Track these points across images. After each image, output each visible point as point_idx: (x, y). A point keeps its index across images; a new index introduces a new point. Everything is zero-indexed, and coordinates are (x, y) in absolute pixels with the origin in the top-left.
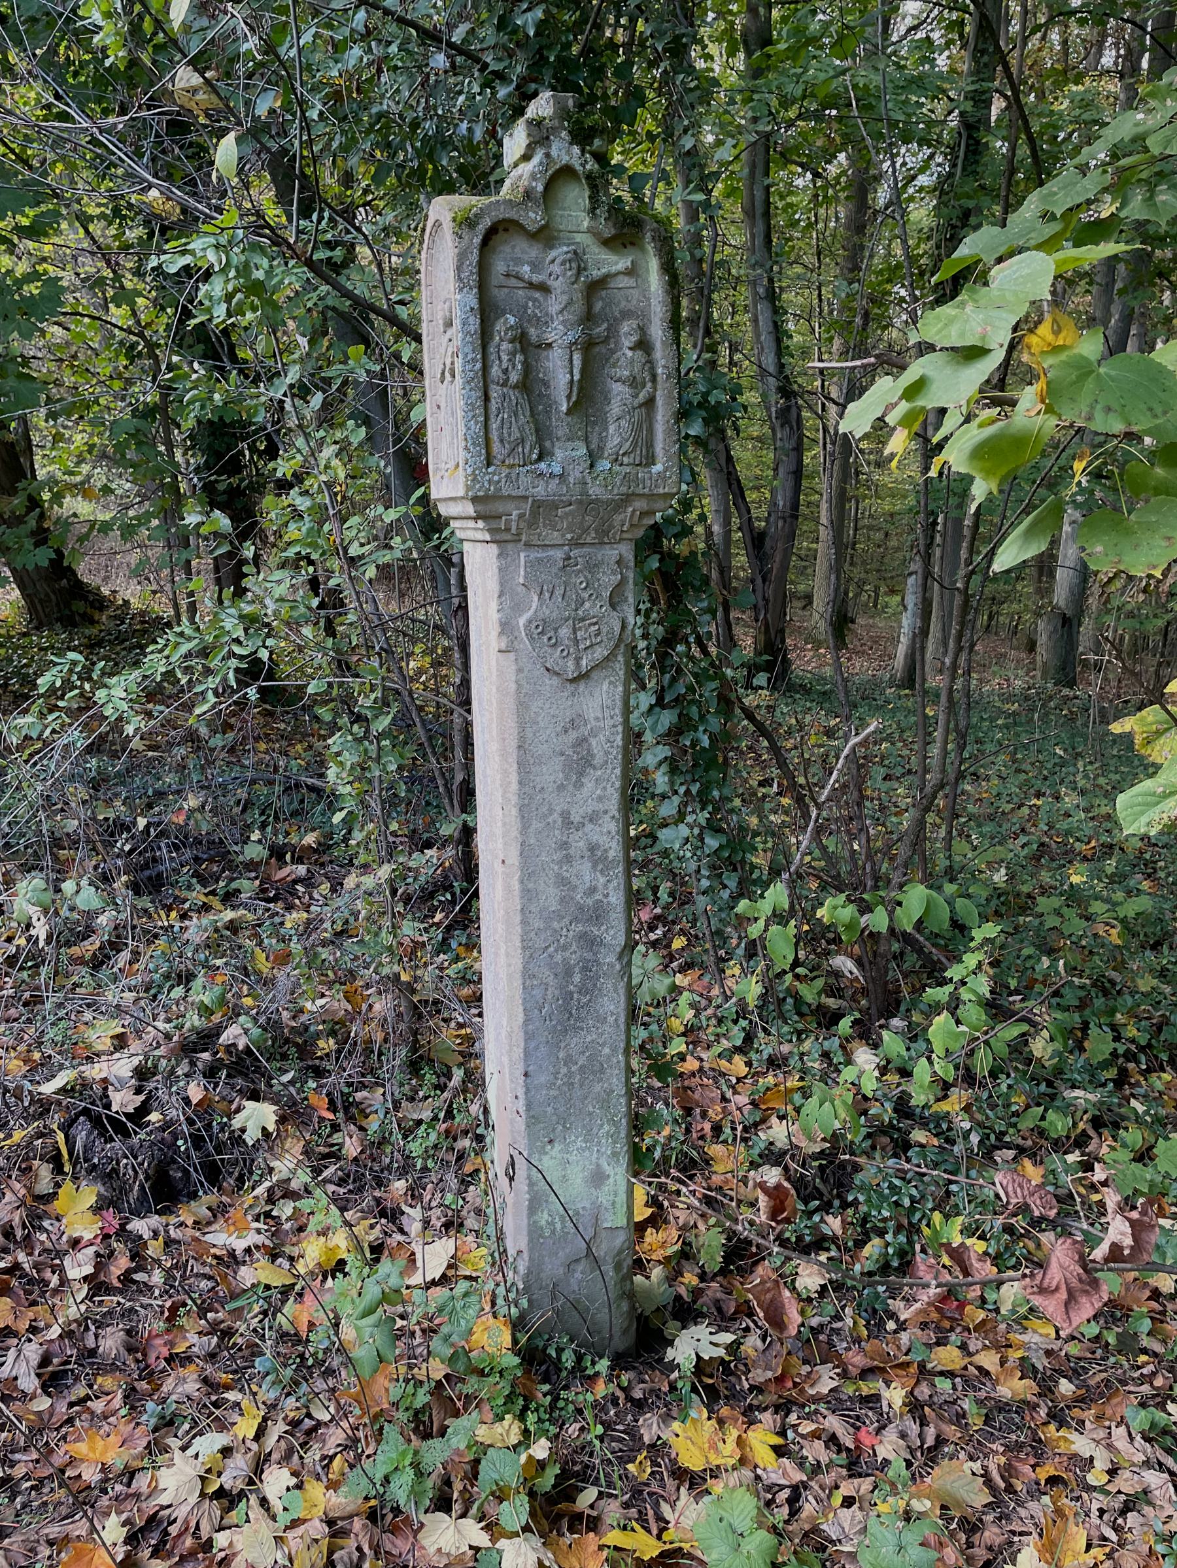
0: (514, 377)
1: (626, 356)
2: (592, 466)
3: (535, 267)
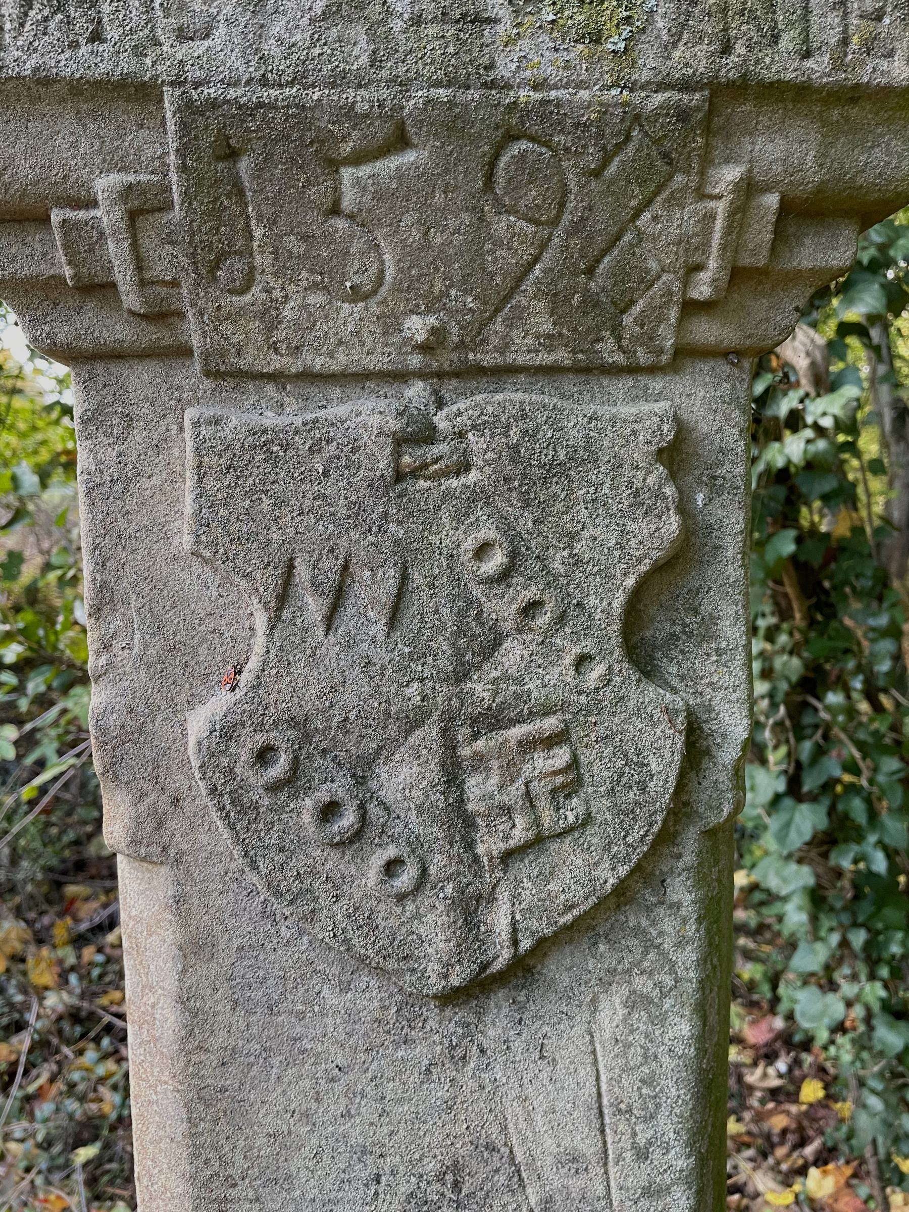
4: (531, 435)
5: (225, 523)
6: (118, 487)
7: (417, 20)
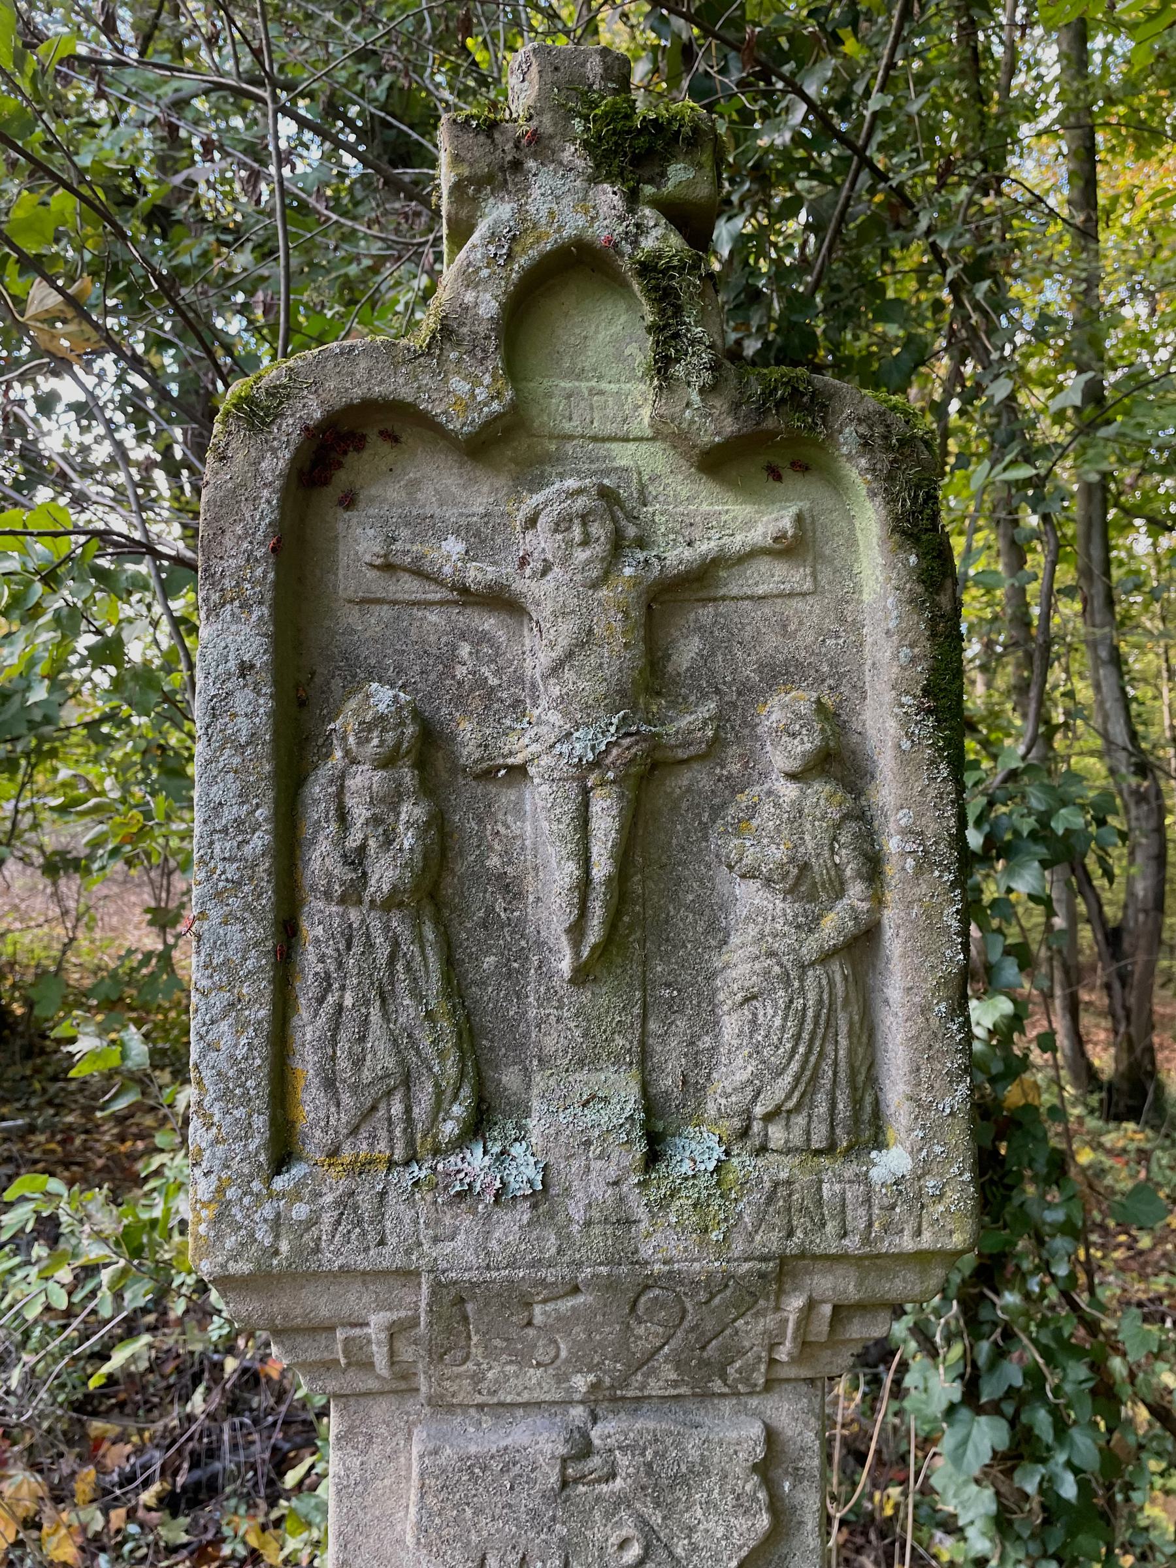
0: (384, 875)
1: (779, 805)
2: (653, 1158)
3: (481, 539)
4: (660, 1455)
5: (438, 1529)
6: (360, 1488)
7: (588, 1224)
